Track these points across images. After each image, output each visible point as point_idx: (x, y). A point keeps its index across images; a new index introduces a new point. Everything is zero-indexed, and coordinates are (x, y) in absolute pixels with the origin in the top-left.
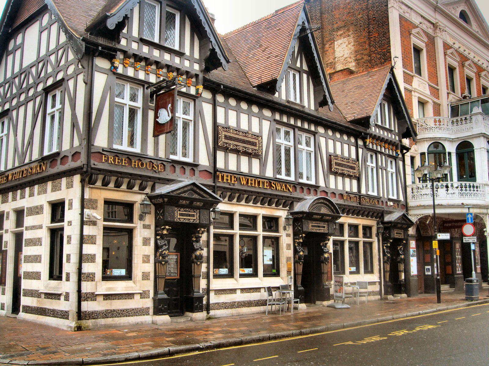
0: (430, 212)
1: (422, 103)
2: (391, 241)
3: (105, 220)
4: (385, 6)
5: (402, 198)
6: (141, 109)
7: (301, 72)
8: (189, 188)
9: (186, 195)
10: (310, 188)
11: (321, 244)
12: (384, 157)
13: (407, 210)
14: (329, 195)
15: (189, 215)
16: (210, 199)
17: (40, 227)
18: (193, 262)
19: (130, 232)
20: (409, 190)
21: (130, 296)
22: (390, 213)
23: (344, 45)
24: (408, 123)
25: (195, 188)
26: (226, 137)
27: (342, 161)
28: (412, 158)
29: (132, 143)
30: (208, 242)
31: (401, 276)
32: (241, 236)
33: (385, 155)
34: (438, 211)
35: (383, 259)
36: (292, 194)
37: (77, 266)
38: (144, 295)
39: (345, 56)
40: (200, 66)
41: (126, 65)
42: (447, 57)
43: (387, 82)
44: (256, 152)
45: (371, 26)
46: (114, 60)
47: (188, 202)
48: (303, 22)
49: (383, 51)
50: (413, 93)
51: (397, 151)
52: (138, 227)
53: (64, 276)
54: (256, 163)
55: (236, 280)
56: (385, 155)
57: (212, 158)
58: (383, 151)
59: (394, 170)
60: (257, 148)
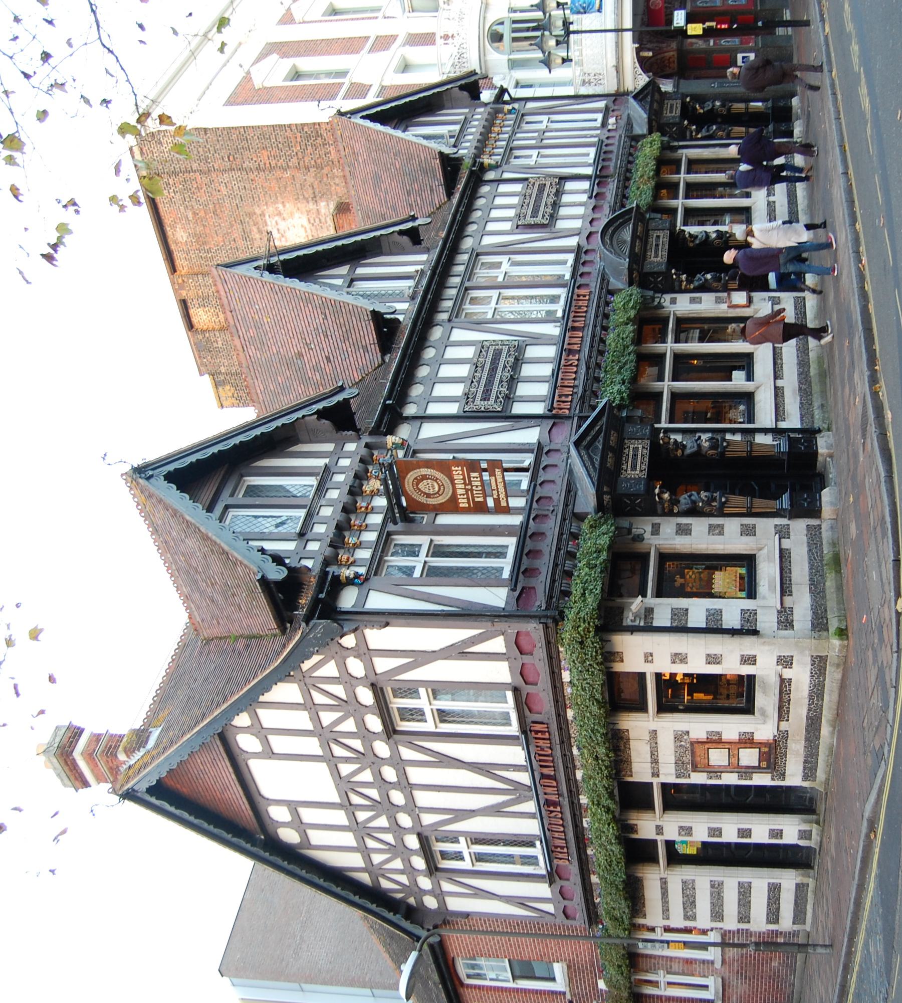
0: (628, 37)
1: (406, 67)
2: (686, 122)
3: (644, 595)
4: (206, 134)
5: (601, 104)
6: (433, 537)
7: (354, 277)
8: (583, 453)
9: (597, 459)
10: (582, 261)
11: (691, 245)
12: (518, 135)
13: (627, 94)
14: (593, 229)
15: (635, 455)
16: (604, 419)
17: (654, 734)
18: (722, 454)
19: (664, 557)
20: (583, 91)
21: (784, 556)
22: (629, 124)
23: (282, 225)
24: (449, 86)
25: (585, 443)
26: (485, 398)
27: (528, 205)
28: (517, 85)
29: (499, 553)
30: (684, 431)
31: (757, 107)
32: (675, 378)
33: (514, 133)
34: (628, 23)
35: (721, 139)
36: (593, 290)
37: (727, 637)
38: (783, 533)
39: (306, 223)
40: (351, 441)
41: (351, 560)
42: (306, 19)
43: (368, 123)
44: (512, 349)
45: (245, 166)
46: (343, 579)
47: (610, 455)
48: (255, 268)
49: (299, 139)
50: (384, 84)
51: (506, 110)
52: (657, 542)
53: (746, 670)
54: (532, 352)
55: (758, 388)
56: (514, 133)
57: (525, 423)
58: (507, 136)
59: (544, 118)
60: (505, 349)
